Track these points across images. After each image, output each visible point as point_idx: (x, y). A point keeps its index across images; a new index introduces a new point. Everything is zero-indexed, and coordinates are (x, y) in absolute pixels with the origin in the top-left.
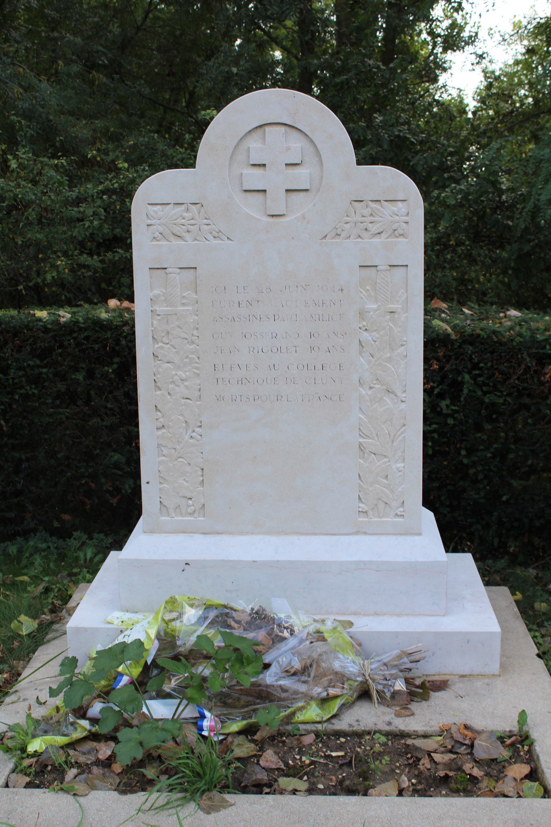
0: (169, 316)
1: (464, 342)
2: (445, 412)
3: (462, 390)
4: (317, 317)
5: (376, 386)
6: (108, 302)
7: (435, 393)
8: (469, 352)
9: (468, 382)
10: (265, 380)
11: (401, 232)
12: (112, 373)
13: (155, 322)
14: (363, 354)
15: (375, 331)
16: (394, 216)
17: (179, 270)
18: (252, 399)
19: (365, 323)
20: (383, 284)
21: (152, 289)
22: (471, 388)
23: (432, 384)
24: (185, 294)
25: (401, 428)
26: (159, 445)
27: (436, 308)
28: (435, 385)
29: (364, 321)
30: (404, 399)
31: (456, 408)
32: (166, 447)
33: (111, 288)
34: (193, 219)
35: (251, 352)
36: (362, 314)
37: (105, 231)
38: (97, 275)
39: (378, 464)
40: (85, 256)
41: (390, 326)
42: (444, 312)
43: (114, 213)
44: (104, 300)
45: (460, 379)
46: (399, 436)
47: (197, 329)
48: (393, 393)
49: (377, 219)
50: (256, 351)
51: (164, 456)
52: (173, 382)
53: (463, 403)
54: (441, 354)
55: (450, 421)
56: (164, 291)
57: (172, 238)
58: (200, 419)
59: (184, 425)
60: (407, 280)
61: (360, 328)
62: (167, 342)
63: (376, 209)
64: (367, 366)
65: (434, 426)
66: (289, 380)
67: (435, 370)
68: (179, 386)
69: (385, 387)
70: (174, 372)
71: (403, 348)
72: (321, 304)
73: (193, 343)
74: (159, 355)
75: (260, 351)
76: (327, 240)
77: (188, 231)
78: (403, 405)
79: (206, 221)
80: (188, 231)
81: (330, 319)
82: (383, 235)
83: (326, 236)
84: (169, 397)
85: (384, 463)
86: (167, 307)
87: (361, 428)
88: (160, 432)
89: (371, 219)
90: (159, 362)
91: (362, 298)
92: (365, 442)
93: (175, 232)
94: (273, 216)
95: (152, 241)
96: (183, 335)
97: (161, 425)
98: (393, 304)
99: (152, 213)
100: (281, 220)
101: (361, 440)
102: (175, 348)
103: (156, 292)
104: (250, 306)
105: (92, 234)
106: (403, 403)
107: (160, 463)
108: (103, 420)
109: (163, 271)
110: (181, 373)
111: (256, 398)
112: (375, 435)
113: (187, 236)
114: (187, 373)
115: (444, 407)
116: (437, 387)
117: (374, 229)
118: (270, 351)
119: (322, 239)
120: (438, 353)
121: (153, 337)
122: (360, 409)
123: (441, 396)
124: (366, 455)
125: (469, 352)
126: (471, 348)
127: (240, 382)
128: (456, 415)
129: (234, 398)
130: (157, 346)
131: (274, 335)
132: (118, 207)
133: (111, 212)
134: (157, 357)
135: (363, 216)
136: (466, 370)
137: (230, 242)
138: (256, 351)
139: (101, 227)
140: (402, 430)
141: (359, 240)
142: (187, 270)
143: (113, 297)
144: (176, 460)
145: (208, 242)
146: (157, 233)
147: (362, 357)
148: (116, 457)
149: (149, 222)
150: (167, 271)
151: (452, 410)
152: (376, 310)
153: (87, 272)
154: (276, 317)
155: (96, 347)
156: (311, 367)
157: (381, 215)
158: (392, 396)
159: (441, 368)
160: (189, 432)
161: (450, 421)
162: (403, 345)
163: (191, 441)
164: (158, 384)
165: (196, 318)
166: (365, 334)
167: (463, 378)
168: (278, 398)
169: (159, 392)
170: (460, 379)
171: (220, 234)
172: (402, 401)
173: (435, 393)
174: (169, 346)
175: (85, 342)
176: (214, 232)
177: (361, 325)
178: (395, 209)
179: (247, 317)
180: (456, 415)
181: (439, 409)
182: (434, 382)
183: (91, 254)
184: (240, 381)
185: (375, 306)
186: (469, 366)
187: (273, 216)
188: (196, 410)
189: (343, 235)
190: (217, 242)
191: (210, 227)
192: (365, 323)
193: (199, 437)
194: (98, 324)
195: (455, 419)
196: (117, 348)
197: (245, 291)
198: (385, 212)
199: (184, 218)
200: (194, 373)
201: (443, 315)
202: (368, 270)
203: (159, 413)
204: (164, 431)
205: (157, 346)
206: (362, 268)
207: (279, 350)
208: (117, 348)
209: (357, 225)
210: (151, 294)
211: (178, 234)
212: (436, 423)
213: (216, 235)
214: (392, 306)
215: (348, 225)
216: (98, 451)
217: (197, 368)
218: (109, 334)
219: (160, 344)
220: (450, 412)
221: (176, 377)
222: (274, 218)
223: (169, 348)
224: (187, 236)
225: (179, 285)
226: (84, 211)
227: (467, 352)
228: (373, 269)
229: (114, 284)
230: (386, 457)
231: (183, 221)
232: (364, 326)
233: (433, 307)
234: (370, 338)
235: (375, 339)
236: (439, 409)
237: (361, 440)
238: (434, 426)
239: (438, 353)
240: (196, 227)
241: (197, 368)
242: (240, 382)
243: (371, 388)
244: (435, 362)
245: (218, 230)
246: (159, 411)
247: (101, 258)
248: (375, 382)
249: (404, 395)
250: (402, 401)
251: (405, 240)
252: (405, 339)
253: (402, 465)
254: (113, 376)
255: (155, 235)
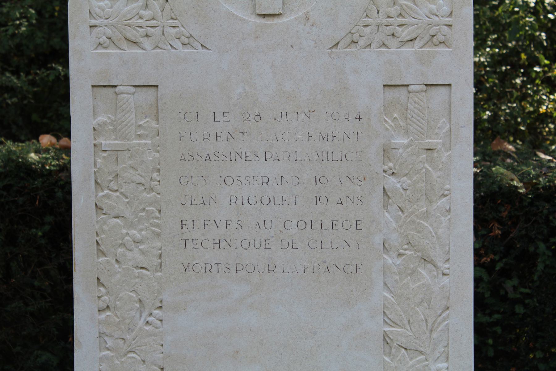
0: (119, 153)
1: (538, 197)
2: (511, 295)
3: (535, 265)
4: (325, 155)
5: (407, 252)
6: (40, 138)
7: (497, 268)
8: (545, 211)
9: (544, 253)
10: (252, 242)
11: (442, 38)
12: (43, 237)
13: (99, 161)
14: (389, 208)
15: (406, 175)
16: (432, 17)
17: (133, 89)
18: (233, 270)
19: (391, 165)
20: (416, 111)
21: (95, 114)
22: (548, 262)
23: (492, 256)
24: (141, 123)
25: (443, 312)
26: (101, 335)
27: (500, 151)
28: (497, 258)
29: (390, 161)
30: (446, 271)
31: (528, 291)
32: (112, 336)
33: (45, 121)
34: (153, 19)
35: (233, 204)
36: (387, 151)
37: (38, 41)
38: (25, 102)
39: (411, 363)
40: (8, 74)
41: (427, 169)
42: (509, 156)
43: (52, 16)
44: (35, 134)
45: (532, 249)
46: (440, 323)
47: (158, 171)
48: (431, 262)
49: (408, 20)
50: (239, 202)
51: (108, 349)
52: (123, 245)
53: (537, 283)
54: (505, 214)
55: (519, 309)
56: (113, 118)
57: (124, 45)
58: (160, 297)
59: (138, 305)
60: (450, 105)
61: (385, 171)
62: (116, 188)
63: (407, 6)
64: (394, 225)
65: (496, 316)
66: (285, 243)
67: (497, 236)
68: (131, 251)
69: (419, 254)
70: (125, 231)
71: (444, 199)
72: (330, 138)
73: (152, 190)
74: (103, 207)
75: (245, 201)
76: (340, 49)
77: (147, 36)
78: (446, 280)
79: (171, 21)
80: (147, 36)
81: (343, 158)
82: (416, 42)
83: (338, 43)
84: (116, 266)
85: (420, 362)
86: (116, 139)
87: (387, 312)
88: (103, 316)
89: (400, 20)
90: (103, 216)
91: (387, 129)
92: (392, 332)
93: (129, 35)
94: (264, 16)
95: (96, 49)
96: (138, 179)
97: (105, 306)
98: (430, 138)
99: (97, 10)
100: (276, 20)
101: (387, 329)
102: (127, 198)
103: (102, 119)
104: (232, 140)
105: (19, 46)
106: (445, 277)
107: (101, 360)
108: (27, 305)
109: (112, 90)
110: (134, 232)
111: (240, 267)
112: (406, 322)
113: (146, 43)
114: (143, 233)
115: (510, 289)
116: (500, 260)
117: (404, 34)
118: (259, 203)
119: (332, 47)
120: (500, 212)
121: (96, 182)
122: (385, 284)
123: (506, 273)
124: (393, 350)
125: (545, 211)
126: (547, 206)
127: (217, 246)
128: (527, 301)
129: (209, 267)
130: (101, 194)
131: (265, 180)
132: (57, 8)
133: (47, 15)
134: (102, 209)
135: (389, 17)
136: (540, 237)
137: (205, 51)
138: (239, 202)
139: (30, 36)
140: (444, 315)
141: (384, 49)
142: (145, 89)
143: (47, 133)
144: (125, 355)
145: (174, 51)
146: (104, 37)
147: (388, 212)
148: (45, 357)
149: (93, 22)
150: (117, 89)
151: (521, 293)
152: (407, 146)
153: (11, 98)
154: (268, 156)
155: (21, 200)
156: (317, 225)
157: (416, 16)
158: (429, 266)
159: (505, 234)
160: (144, 315)
161: (519, 309)
162: (444, 196)
163: (147, 328)
164: (102, 247)
165: (157, 155)
166: (392, 179)
167: (537, 248)
168: (271, 268)
169: (102, 259)
170: (532, 249)
171: (191, 40)
172: (444, 274)
173: (497, 268)
174: (118, 194)
175: (5, 193)
176: (183, 38)
177: (386, 167)
178: (433, 6)
179: (228, 155)
180: (527, 301)
181: (502, 292)
182: (495, 254)
183: (16, 73)
184: (217, 245)
185: (406, 141)
186: (546, 231)
187: (264, 16)
188: (155, 284)
189: (362, 42)
190: (187, 50)
191: (177, 29)
192: (391, 165)
193: (159, 322)
194: (28, 170)
195: (526, 306)
196: (50, 202)
197: (226, 119)
198: (419, 11)
199: (141, 18)
200: (153, 232)
201: (509, 161)
202: (396, 91)
203: (102, 289)
204: (108, 313)
205: (101, 194)
206: (387, 89)
207: (272, 201)
208: (50, 202)
209: (380, 29)
210: (94, 122)
211: (133, 39)
212: (498, 312)
213: (186, 41)
214: (429, 142)
215: (368, 28)
216: (18, 349)
217: (157, 226)
218: (38, 183)
219: (106, 192)
220: (518, 296)
221: (127, 238)
222: (266, 18)
223: (118, 197)
224: (146, 43)
225: (133, 110)
226: (8, 12)
227: (542, 212)
228: (403, 90)
229: (49, 115)
230: (421, 353)
231: (140, 21)
232: (390, 169)
233: (495, 149)
234: (399, 186)
235: (405, 187)
236: (502, 292)
237: (387, 329)
238: (496, 316)
239: (500, 212)
240: (158, 30)
241: (157, 226)
242: (217, 246)
243: (400, 255)
244: (496, 225)
245: (188, 35)
246: (103, 286)
247: (30, 77)
248: (406, 246)
249: (447, 266)
250: (444, 274)
251: (447, 49)
252: (447, 186)
253: (445, 365)
254: (43, 242)
255: (101, 40)
